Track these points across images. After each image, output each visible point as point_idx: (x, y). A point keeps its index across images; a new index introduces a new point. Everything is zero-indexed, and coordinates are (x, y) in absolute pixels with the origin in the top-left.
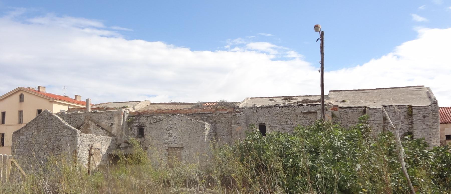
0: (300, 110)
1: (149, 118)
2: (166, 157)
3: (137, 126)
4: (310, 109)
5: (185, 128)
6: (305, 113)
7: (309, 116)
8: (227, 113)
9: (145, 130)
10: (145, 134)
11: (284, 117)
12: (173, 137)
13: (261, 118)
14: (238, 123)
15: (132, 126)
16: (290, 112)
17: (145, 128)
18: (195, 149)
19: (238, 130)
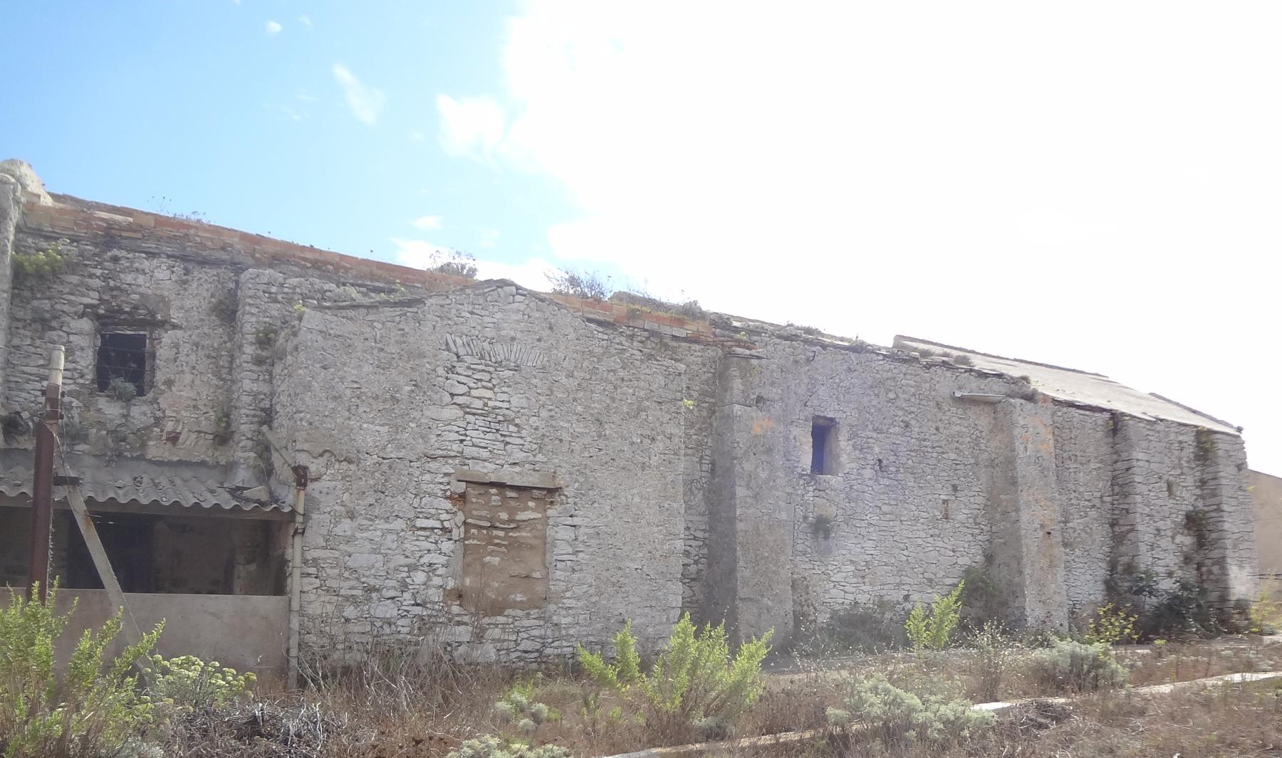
0: (946, 384)
1: (197, 273)
2: (447, 546)
3: (88, 312)
4: (974, 385)
5: (570, 375)
6: (962, 399)
7: (973, 412)
8: (686, 340)
9: (163, 352)
10: (160, 377)
11: (898, 403)
12: (499, 421)
13: (822, 391)
14: (760, 399)
15: (46, 305)
16: (918, 387)
17: (167, 337)
18: (627, 507)
19: (759, 431)
